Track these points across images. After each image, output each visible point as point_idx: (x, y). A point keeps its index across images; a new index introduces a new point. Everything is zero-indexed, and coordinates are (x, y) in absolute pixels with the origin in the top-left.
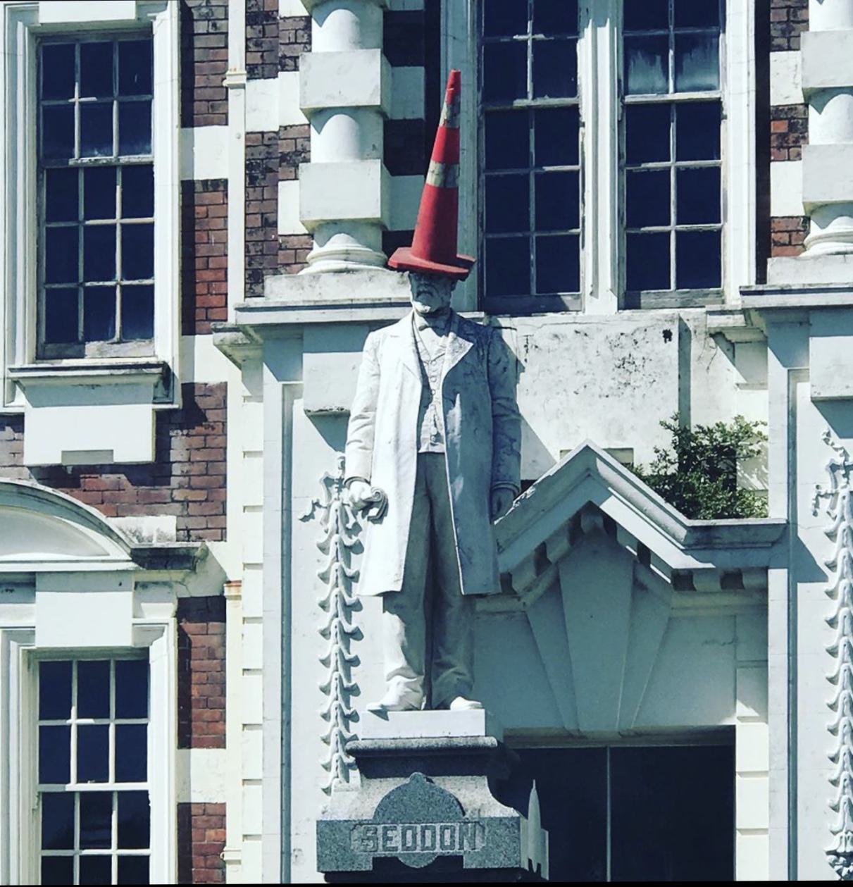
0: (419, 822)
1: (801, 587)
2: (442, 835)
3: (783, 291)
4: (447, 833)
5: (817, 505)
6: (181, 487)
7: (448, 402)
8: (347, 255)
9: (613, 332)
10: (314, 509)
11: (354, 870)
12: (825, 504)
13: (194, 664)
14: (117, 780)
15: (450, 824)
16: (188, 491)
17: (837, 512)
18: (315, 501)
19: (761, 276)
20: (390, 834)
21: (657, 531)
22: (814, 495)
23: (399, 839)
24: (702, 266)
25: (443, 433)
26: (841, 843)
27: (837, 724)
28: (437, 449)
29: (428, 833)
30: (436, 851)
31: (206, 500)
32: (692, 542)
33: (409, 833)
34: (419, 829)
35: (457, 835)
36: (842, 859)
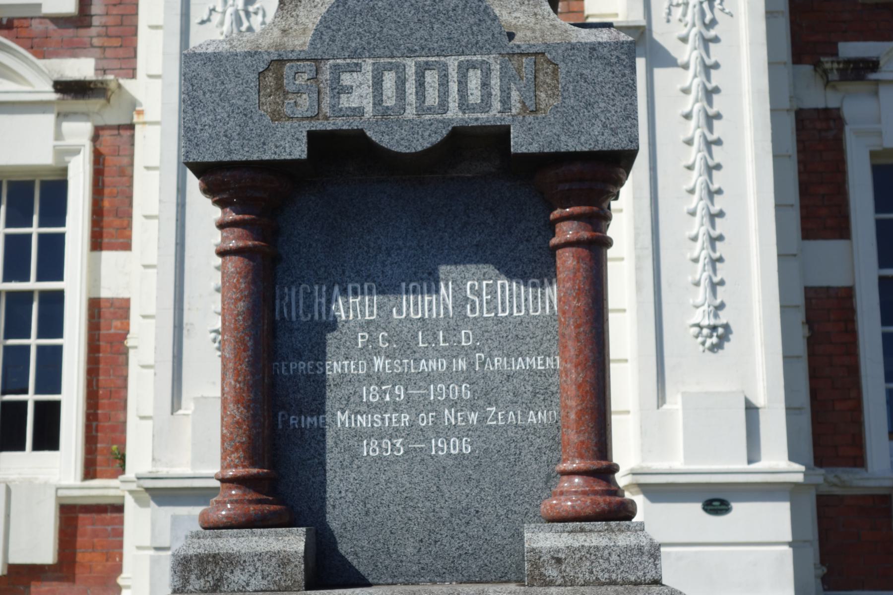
0: (411, 53)
2: (463, 83)
4: (474, 80)
5: (669, 14)
6: (99, 36)
10: (210, 14)
11: (266, 157)
12: (678, 12)
13: (108, 179)
14: (40, 278)
15: (479, 58)
16: (105, 39)
17: (689, 18)
18: (212, 7)
20: (346, 79)
23: (367, 90)
26: (704, 316)
27: (696, 208)
29: (431, 78)
30: (450, 115)
31: (121, 46)
33: (389, 80)
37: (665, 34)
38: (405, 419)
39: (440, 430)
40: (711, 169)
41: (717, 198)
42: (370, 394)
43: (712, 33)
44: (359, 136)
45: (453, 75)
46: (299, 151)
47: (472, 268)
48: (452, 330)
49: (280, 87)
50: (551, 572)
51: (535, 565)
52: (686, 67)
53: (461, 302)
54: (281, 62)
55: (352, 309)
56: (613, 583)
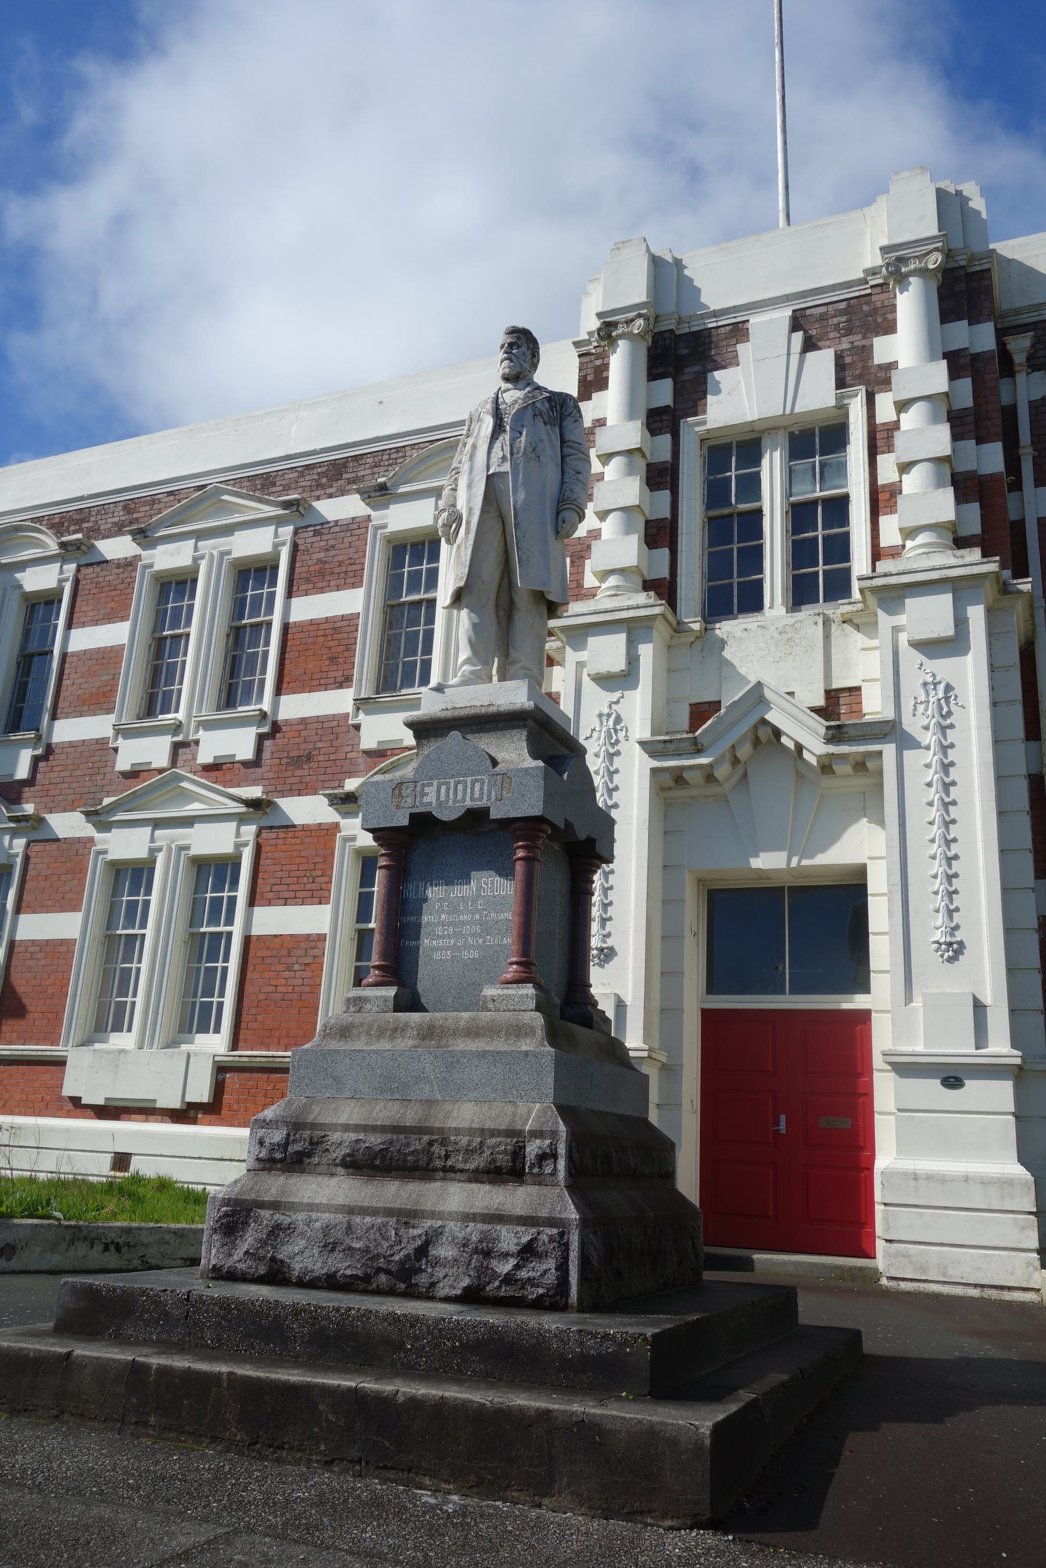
0: (453, 777)
1: (905, 752)
3: (885, 575)
4: (477, 786)
5: (915, 709)
7: (517, 432)
8: (617, 587)
9: (780, 624)
12: (921, 708)
17: (929, 712)
19: (874, 570)
21: (809, 737)
22: (913, 703)
23: (434, 794)
24: (839, 586)
25: (508, 456)
28: (502, 469)
29: (460, 787)
32: (829, 737)
34: (452, 784)
35: (486, 787)
36: (943, 947)
37: (911, 725)
38: (452, 941)
39: (468, 947)
40: (947, 824)
41: (953, 845)
42: (439, 931)
43: (949, 722)
44: (429, 815)
45: (469, 785)
46: (405, 822)
47: (485, 872)
48: (474, 901)
49: (400, 794)
50: (490, 1006)
51: (485, 1002)
52: (928, 748)
53: (479, 888)
54: (402, 783)
55: (434, 893)
56: (515, 1010)
